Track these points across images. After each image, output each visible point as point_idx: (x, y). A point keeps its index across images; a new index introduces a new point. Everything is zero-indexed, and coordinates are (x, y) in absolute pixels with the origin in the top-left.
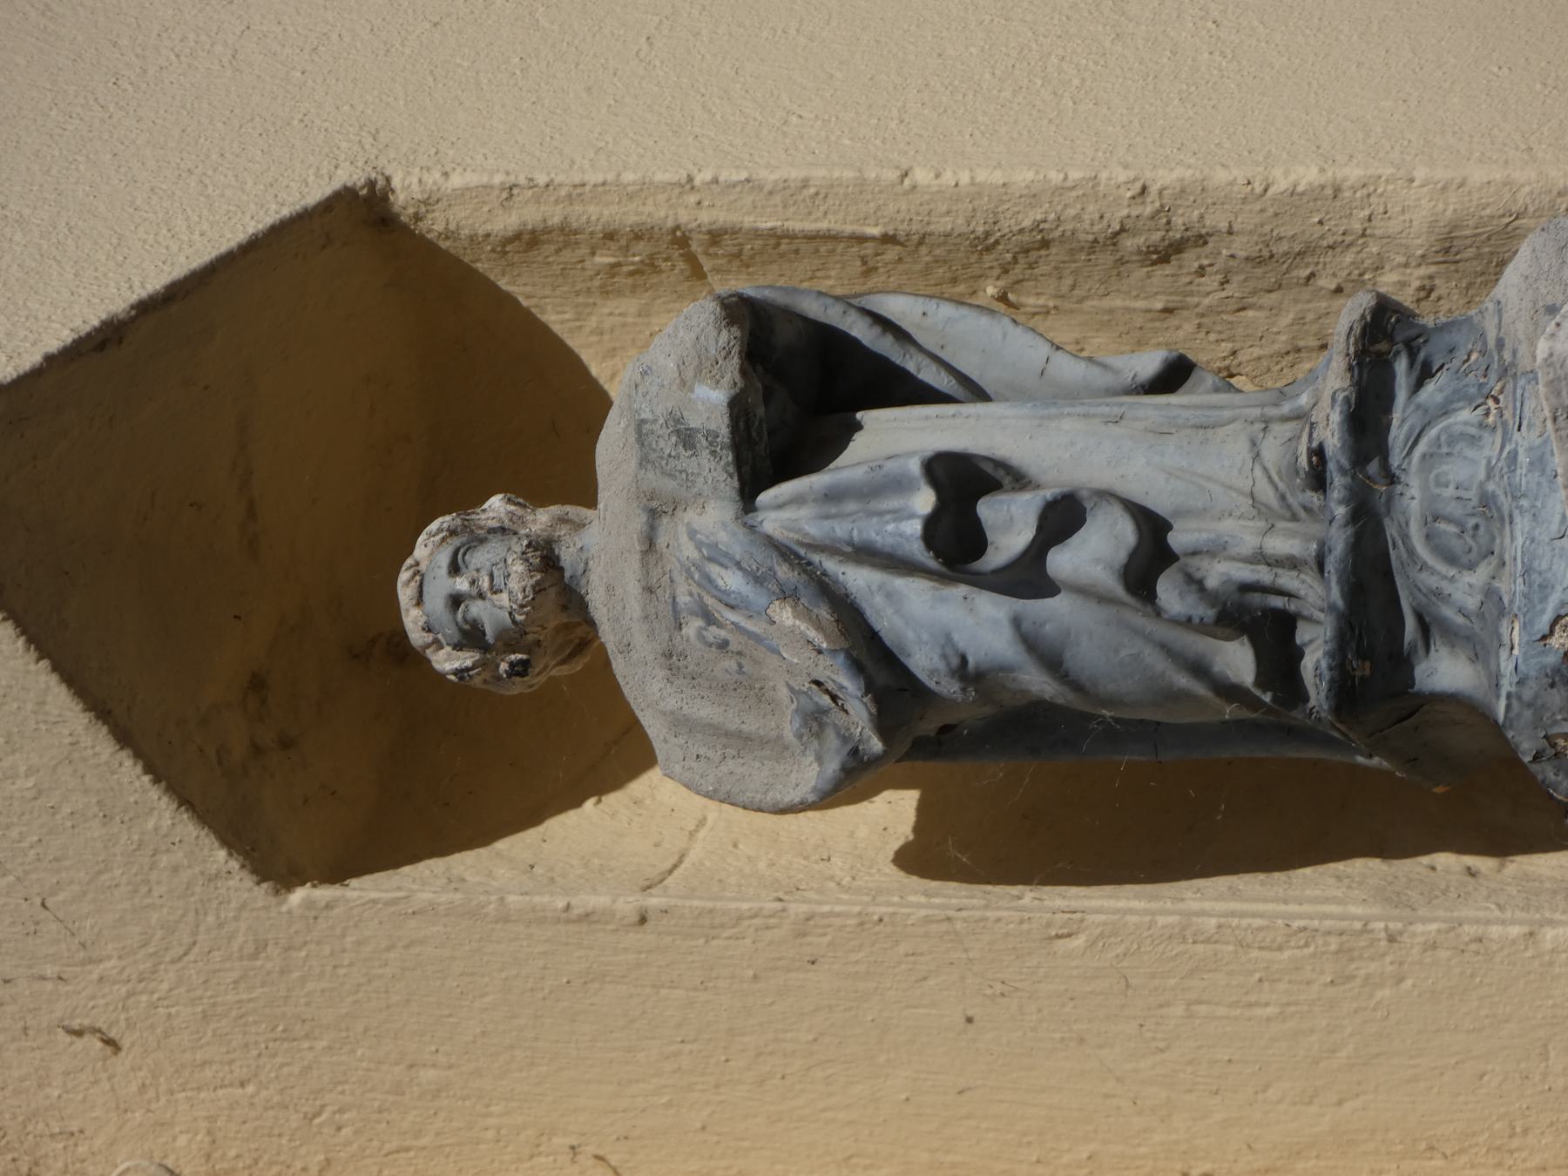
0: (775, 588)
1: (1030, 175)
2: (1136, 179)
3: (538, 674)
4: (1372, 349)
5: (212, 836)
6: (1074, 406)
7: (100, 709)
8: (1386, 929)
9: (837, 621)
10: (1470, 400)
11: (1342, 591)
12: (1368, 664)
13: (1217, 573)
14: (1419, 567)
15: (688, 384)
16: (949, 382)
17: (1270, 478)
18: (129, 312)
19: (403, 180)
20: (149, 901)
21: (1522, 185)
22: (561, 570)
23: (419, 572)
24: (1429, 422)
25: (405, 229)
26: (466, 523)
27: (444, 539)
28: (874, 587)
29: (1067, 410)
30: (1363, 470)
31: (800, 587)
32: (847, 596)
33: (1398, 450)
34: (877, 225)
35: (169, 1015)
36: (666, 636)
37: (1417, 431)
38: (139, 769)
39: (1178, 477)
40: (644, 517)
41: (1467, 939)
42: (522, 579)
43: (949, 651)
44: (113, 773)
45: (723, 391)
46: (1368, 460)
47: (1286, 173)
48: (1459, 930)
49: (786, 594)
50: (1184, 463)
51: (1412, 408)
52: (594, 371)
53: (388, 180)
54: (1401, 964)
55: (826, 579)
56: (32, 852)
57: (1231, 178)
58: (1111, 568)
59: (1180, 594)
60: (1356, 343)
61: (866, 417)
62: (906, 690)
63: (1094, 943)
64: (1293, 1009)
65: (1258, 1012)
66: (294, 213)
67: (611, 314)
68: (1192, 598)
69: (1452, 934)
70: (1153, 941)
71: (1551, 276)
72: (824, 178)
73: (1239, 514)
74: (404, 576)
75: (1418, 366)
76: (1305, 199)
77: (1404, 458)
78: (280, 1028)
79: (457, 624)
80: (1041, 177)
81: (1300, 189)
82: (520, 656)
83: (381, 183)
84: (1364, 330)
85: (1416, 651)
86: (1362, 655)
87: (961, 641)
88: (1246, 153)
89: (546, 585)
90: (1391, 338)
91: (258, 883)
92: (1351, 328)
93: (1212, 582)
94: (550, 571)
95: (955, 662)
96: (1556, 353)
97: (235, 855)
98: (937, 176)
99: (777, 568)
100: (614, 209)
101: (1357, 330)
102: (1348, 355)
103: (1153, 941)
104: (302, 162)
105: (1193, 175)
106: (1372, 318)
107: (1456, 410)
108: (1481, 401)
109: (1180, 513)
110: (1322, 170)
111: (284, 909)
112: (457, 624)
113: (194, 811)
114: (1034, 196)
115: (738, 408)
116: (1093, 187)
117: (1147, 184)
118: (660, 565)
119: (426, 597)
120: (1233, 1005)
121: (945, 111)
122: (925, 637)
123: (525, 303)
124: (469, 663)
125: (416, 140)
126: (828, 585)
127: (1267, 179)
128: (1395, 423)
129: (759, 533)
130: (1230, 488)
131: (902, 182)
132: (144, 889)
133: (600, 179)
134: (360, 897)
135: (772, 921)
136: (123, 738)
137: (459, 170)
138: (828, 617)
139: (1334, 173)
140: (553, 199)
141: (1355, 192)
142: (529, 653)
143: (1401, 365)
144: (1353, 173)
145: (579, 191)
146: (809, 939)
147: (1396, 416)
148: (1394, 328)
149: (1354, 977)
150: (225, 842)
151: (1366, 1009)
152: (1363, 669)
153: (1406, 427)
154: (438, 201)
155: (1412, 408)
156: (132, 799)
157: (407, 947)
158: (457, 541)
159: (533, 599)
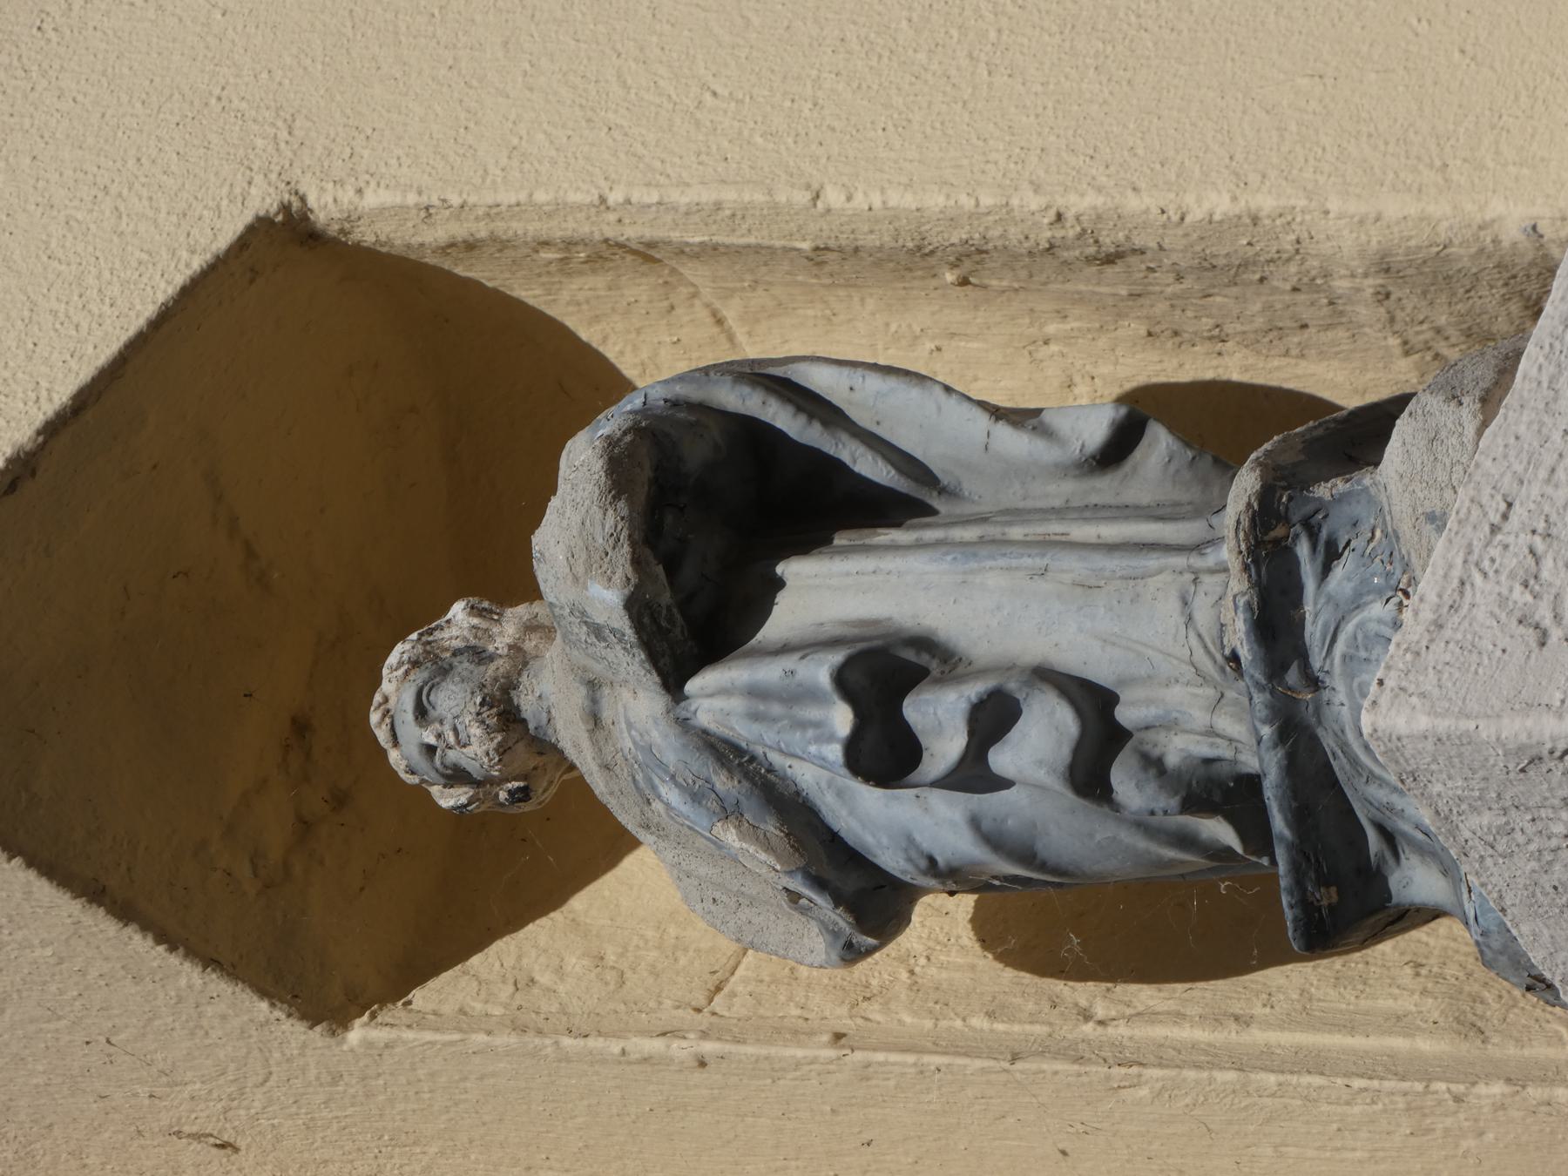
0: (714, 806)
1: (941, 200)
2: (1048, 207)
3: (544, 791)
4: (1266, 538)
5: (248, 990)
6: (995, 560)
7: (94, 892)
8: (1449, 1090)
9: (787, 835)
10: (1379, 591)
11: (1286, 819)
12: (1333, 890)
13: (1178, 749)
14: (1364, 780)
15: (581, 581)
16: (888, 473)
17: (1205, 647)
18: (36, 440)
19: (319, 199)
20: (207, 1042)
21: (1439, 221)
22: (524, 721)
23: (388, 711)
24: (1343, 618)
25: (335, 241)
26: (428, 648)
27: (407, 673)
28: (824, 785)
29: (990, 563)
30: (1282, 681)
31: (742, 799)
32: (798, 793)
33: (1317, 650)
34: (805, 240)
35: (273, 1126)
36: (637, 810)
37: (1332, 629)
38: (150, 941)
39: (1114, 644)
40: (583, 691)
41: (1534, 1102)
42: (481, 743)
43: (914, 855)
44: (126, 944)
45: (616, 592)
46: (1285, 668)
47: (1199, 201)
48: (1524, 1094)
49: (728, 812)
50: (1116, 629)
51: (1322, 600)
52: (584, 335)
53: (303, 199)
54: (1476, 1120)
55: (771, 777)
56: (77, 1003)
57: (1143, 207)
58: (1054, 771)
59: (1137, 786)
60: (1247, 539)
61: (792, 569)
62: (883, 887)
63: (1159, 1094)
64: (1381, 1154)
65: (1349, 1155)
66: (205, 265)
67: (580, 289)
68: (1151, 788)
69: (1517, 1098)
70: (1218, 1095)
71: (1425, 478)
72: (735, 201)
73: (1185, 680)
74: (374, 717)
75: (1321, 547)
76: (1226, 226)
77: (1325, 659)
78: (386, 1138)
79: (437, 770)
80: (952, 202)
81: (1217, 217)
82: (516, 784)
83: (296, 205)
84: (1253, 520)
85: (1385, 862)
86: (1323, 881)
87: (926, 842)
88: (1158, 167)
89: (510, 744)
90: (1286, 520)
91: (311, 1028)
92: (1238, 522)
93: (1172, 760)
94: (512, 726)
95: (923, 863)
96: (1379, 729)
97: (278, 1003)
98: (849, 199)
99: (714, 778)
100: (537, 225)
101: (1245, 523)
102: (1241, 552)
103: (1218, 1095)
104: (217, 174)
105: (1105, 204)
106: (1259, 505)
107: (1366, 604)
108: (1390, 594)
109: (1122, 682)
110: (1234, 199)
111: (345, 1048)
112: (437, 770)
113: (222, 969)
114: (952, 219)
115: (636, 606)
116: (1008, 213)
117: (1062, 210)
118: (610, 742)
119: (401, 740)
120: (1322, 1148)
121: (859, 87)
122: (885, 841)
123: (490, 284)
124: (463, 800)
125: (332, 135)
126: (774, 784)
127: (1180, 207)
128: (1309, 618)
129: (694, 727)
130: (1169, 655)
131: (815, 205)
132: (201, 1033)
133: (513, 201)
134: (415, 1040)
135: (832, 1067)
136: (125, 912)
137: (373, 184)
138: (778, 832)
139: (1247, 202)
140: (472, 217)
141: (1274, 220)
142: (525, 777)
143: (1303, 549)
144: (1266, 203)
145: (494, 211)
146: (873, 1082)
147: (1309, 608)
148: (1287, 509)
149: (1434, 1130)
150: (263, 993)
151: (1456, 1156)
152: (1327, 897)
153: (1320, 623)
154: (359, 218)
155: (1322, 600)
156: (155, 964)
157: (481, 1078)
158: (419, 676)
159: (500, 760)
